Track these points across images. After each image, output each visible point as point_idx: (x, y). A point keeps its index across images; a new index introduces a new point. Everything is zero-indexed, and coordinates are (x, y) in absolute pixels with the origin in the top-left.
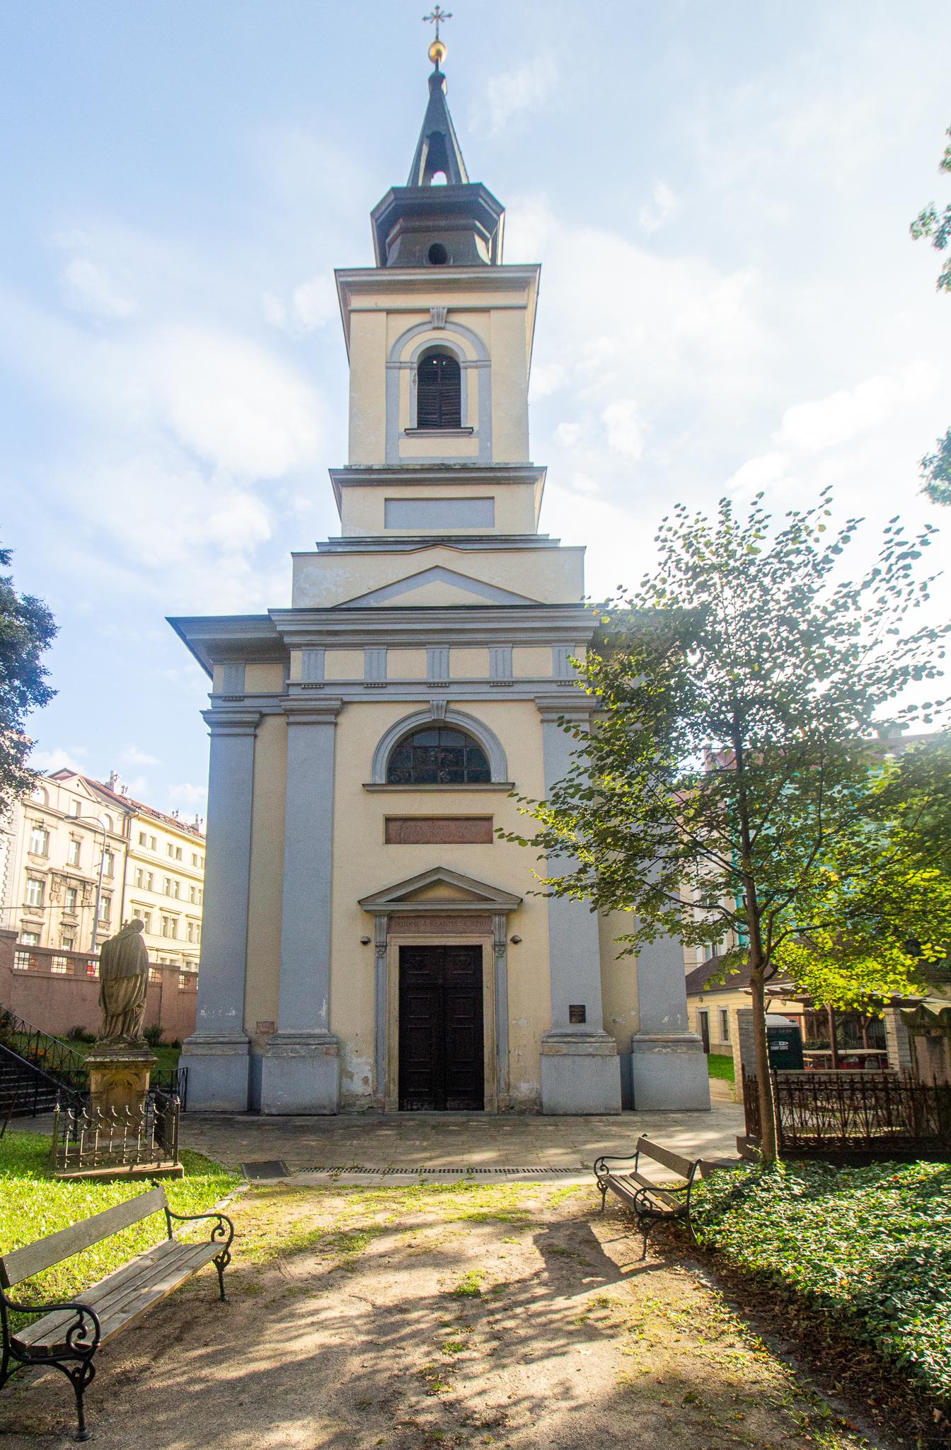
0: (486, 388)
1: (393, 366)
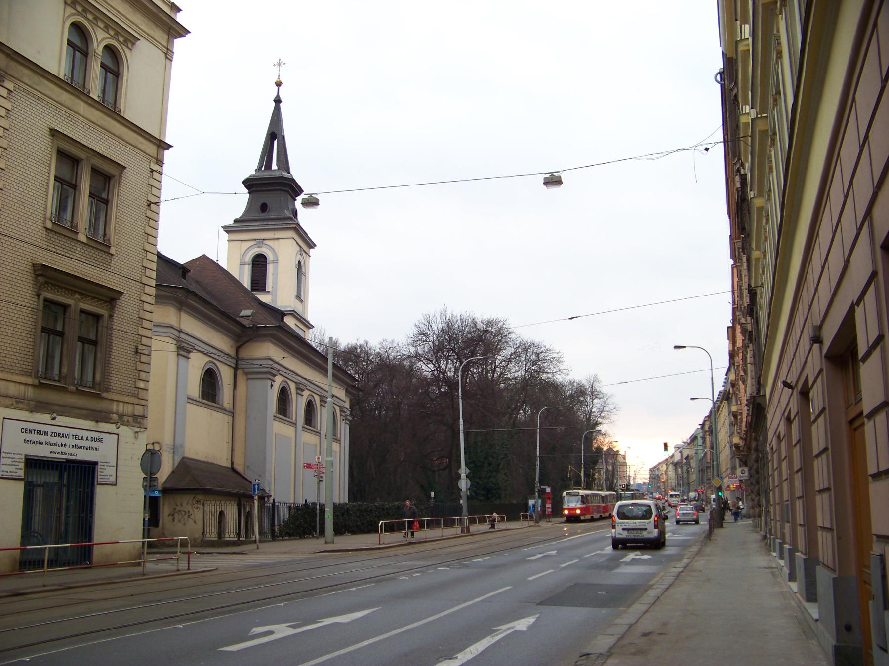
1: (242, 264)
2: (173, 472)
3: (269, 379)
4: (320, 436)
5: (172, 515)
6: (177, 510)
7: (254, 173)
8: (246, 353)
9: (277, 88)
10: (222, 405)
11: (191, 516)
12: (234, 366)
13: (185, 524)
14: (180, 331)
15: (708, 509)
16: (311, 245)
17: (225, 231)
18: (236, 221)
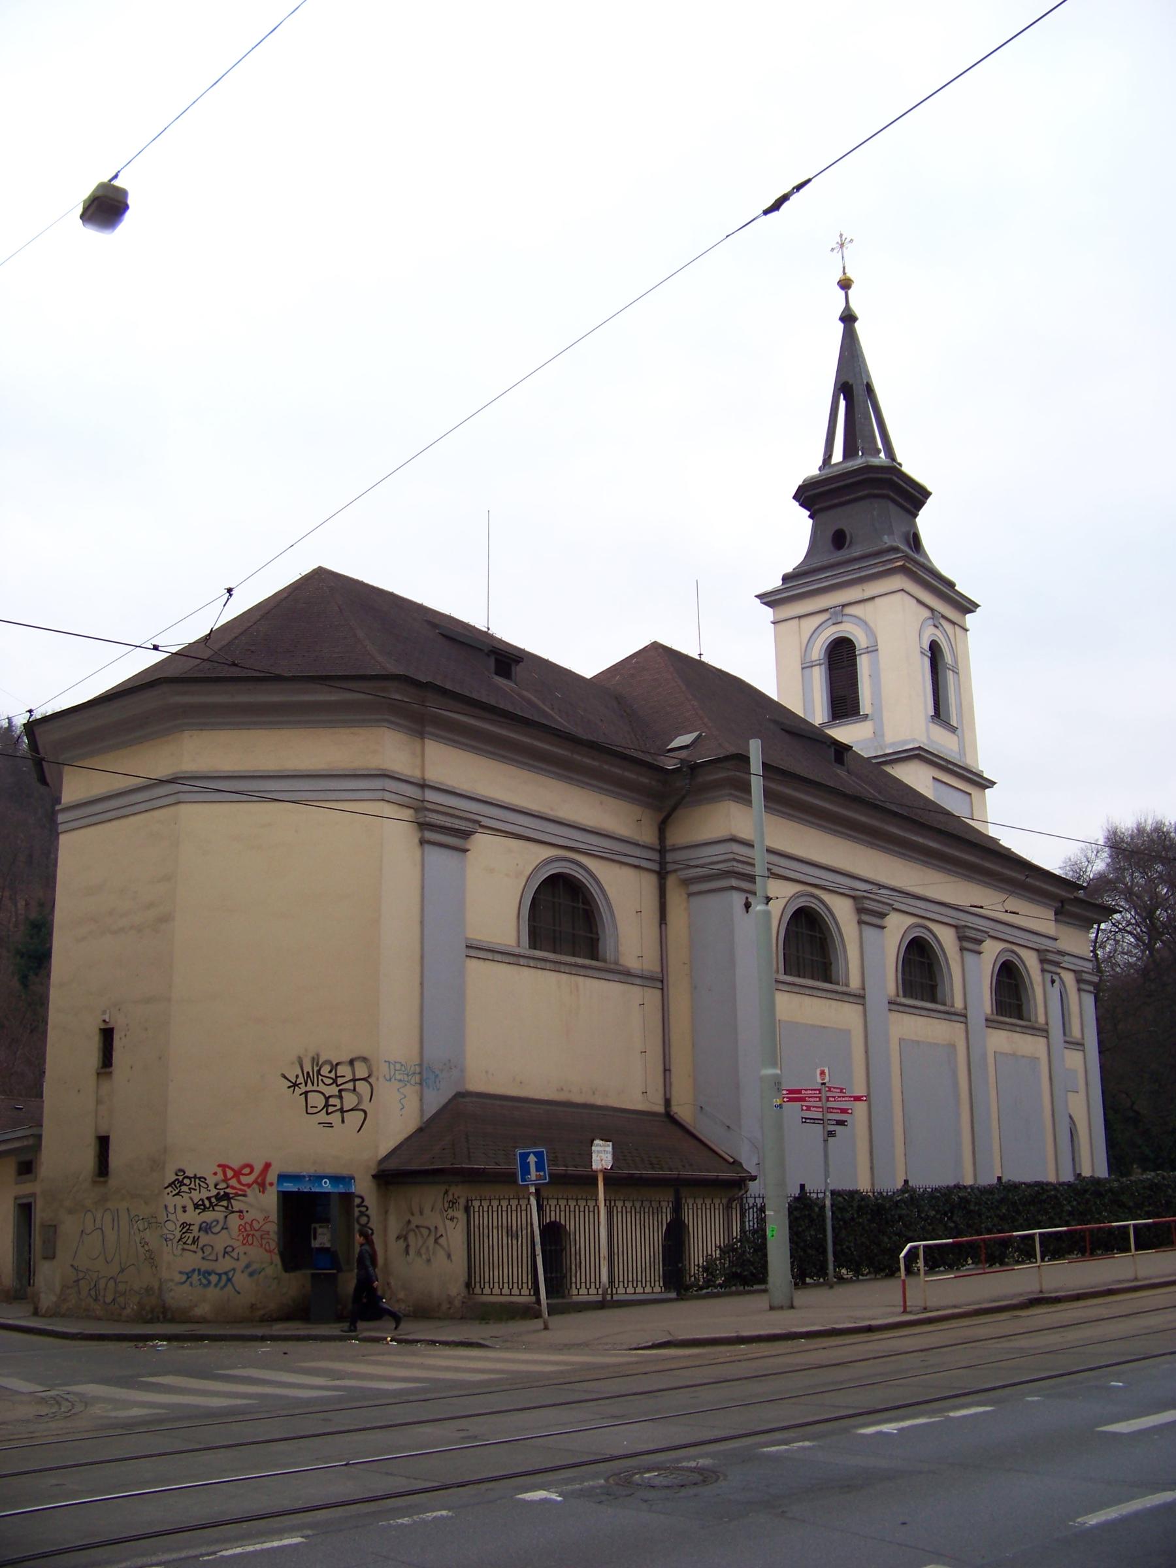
0: (875, 666)
1: (806, 666)
2: (420, 1130)
3: (733, 888)
4: (966, 1023)
5: (402, 1237)
6: (413, 1226)
7: (819, 472)
8: (678, 836)
9: (842, 293)
10: (616, 963)
11: (442, 1241)
12: (656, 867)
13: (429, 1261)
14: (423, 786)
15: (775, 1230)
16: (967, 606)
17: (765, 604)
18: (786, 578)
